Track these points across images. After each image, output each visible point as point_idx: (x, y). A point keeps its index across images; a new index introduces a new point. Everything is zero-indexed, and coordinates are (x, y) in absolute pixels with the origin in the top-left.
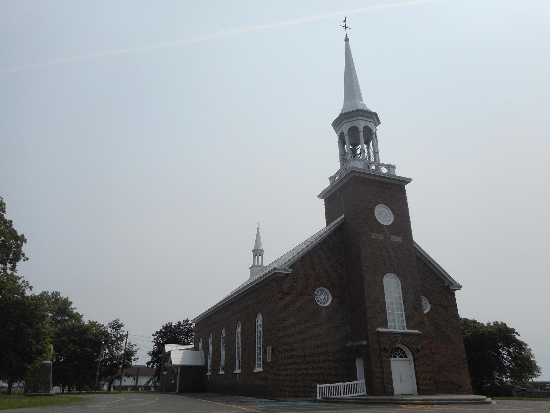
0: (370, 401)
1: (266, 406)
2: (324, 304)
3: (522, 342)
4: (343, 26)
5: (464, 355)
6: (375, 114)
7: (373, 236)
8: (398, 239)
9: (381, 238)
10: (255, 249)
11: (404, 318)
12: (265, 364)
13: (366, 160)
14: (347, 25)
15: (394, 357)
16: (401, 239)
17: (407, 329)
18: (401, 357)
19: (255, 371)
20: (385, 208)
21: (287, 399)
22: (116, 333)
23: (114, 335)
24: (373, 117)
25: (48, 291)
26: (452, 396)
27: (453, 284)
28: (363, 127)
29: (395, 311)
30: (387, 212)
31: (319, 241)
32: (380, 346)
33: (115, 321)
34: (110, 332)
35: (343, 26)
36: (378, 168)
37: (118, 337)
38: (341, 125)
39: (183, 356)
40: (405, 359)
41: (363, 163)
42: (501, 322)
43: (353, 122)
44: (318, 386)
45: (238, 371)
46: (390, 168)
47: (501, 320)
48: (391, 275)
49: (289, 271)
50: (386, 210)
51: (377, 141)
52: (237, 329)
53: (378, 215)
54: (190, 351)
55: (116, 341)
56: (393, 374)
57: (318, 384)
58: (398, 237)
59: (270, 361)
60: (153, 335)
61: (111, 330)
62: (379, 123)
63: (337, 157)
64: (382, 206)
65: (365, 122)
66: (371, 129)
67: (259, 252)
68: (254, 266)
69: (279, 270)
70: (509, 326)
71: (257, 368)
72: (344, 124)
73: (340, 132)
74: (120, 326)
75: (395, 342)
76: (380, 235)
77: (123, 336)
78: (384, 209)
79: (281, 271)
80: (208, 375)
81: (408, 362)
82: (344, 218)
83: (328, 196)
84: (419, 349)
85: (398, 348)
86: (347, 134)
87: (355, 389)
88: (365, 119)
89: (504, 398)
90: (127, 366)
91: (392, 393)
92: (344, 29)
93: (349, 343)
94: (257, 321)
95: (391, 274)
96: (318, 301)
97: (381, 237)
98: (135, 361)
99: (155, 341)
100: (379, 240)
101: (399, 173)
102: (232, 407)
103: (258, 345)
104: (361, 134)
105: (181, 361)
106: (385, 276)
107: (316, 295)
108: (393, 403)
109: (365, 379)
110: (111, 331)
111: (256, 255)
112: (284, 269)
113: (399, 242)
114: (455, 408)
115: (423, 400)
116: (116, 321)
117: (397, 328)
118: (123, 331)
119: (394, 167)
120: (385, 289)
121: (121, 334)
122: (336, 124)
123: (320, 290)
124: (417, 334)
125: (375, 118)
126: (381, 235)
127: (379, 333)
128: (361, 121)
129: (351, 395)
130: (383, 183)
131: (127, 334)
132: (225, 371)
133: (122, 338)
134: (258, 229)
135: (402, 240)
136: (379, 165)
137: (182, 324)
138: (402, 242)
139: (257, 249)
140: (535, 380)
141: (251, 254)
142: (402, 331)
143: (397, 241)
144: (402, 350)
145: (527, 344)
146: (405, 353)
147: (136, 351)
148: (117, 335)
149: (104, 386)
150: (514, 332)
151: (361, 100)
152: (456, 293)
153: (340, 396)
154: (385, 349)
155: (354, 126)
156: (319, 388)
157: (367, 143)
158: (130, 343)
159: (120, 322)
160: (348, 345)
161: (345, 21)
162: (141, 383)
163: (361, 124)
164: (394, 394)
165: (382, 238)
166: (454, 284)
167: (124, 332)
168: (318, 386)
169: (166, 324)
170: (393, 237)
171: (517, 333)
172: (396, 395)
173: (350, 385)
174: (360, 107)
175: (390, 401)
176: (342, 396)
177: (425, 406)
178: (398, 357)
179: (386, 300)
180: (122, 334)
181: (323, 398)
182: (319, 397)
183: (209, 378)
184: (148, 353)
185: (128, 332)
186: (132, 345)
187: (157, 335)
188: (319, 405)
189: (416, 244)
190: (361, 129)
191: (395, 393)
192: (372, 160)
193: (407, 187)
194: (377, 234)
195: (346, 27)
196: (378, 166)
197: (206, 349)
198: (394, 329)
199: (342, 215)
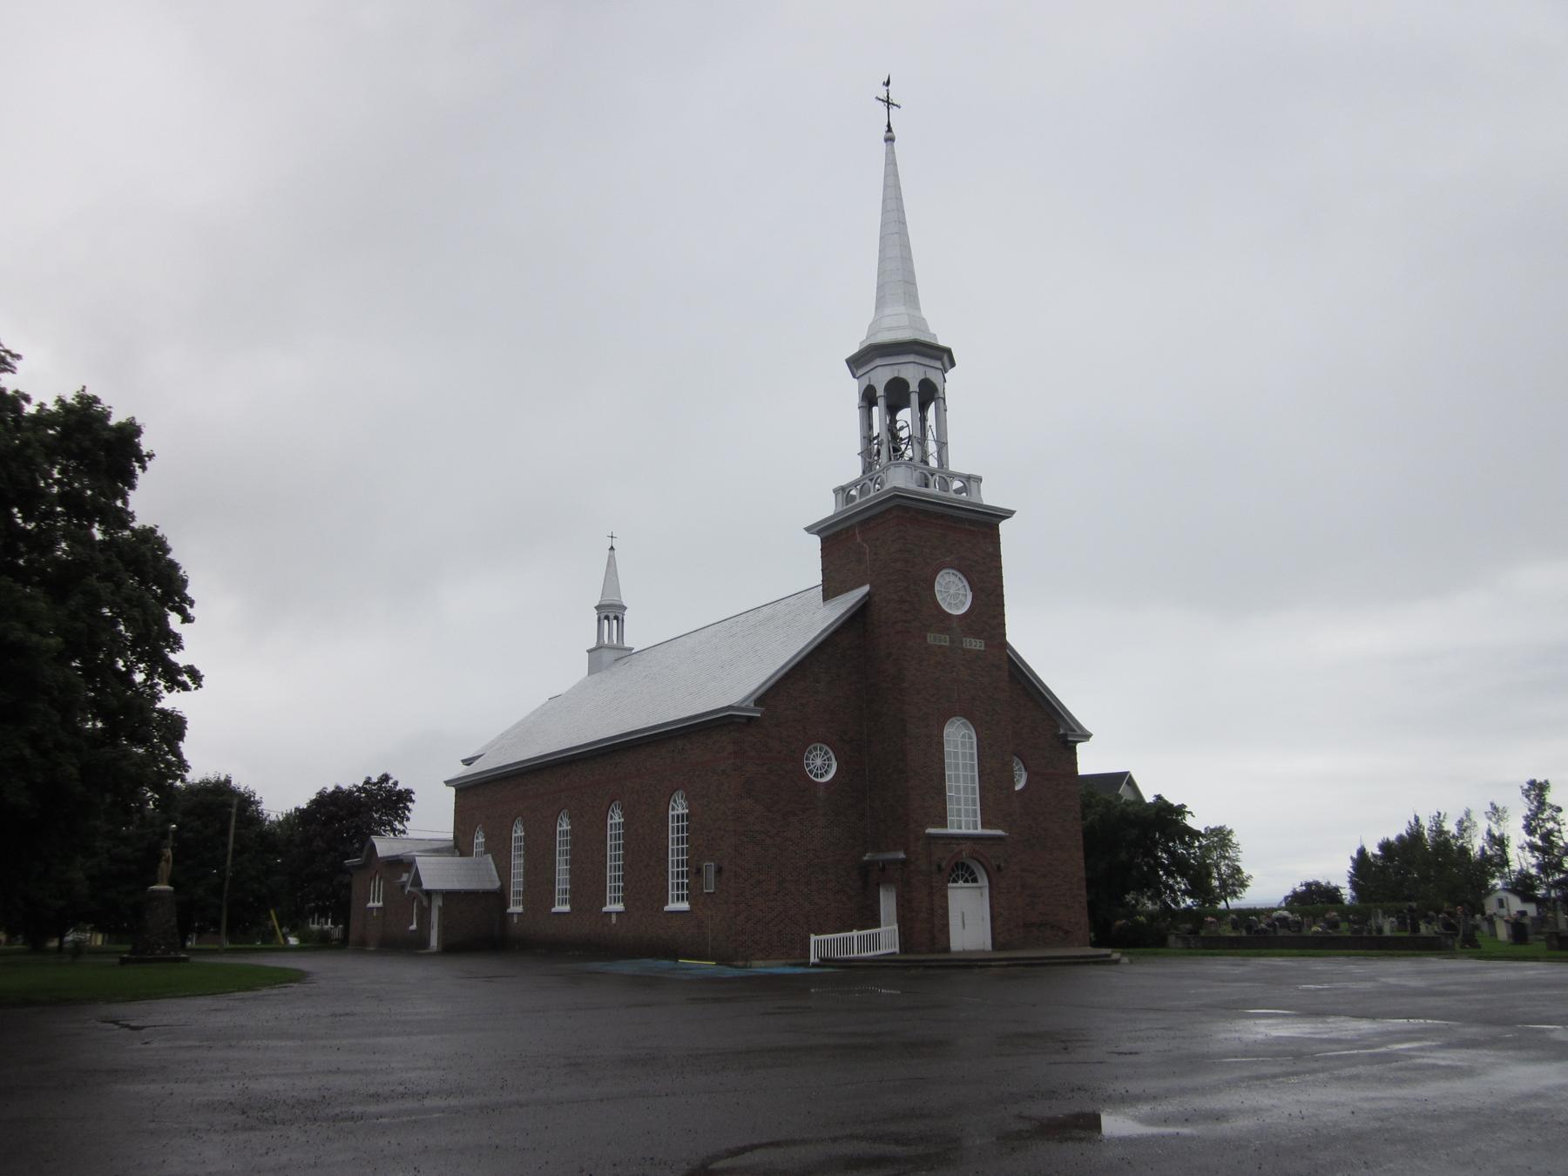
2: (821, 777)
5: (1083, 874)
6: (948, 352)
7: (928, 640)
8: (977, 645)
9: (943, 644)
14: (894, 98)
15: (955, 881)
16: (983, 644)
17: (983, 827)
18: (966, 881)
24: (942, 356)
27: (1074, 731)
28: (918, 381)
29: (962, 793)
30: (961, 585)
40: (974, 885)
43: (896, 367)
44: (813, 938)
50: (957, 580)
51: (946, 410)
56: (950, 914)
58: (978, 641)
59: (712, 891)
62: (953, 364)
64: (949, 573)
65: (922, 369)
68: (600, 647)
71: (673, 902)
73: (865, 382)
78: (953, 578)
80: (513, 914)
81: (978, 891)
82: (868, 594)
84: (1002, 865)
86: (882, 394)
91: (947, 949)
92: (882, 107)
96: (811, 771)
97: (944, 641)
100: (940, 647)
101: (990, 496)
124: (999, 838)
127: (931, 837)
135: (986, 645)
136: (947, 477)
138: (985, 651)
140: (1234, 903)
142: (971, 831)
144: (974, 874)
152: (1080, 747)
157: (923, 407)
161: (888, 83)
163: (912, 374)
164: (486, 894)
166: (1076, 729)
168: (813, 938)
175: (893, 964)
189: (1012, 648)
191: (497, 884)
192: (933, 463)
193: (1004, 527)
194: (938, 635)
195: (888, 103)
199: (863, 584)
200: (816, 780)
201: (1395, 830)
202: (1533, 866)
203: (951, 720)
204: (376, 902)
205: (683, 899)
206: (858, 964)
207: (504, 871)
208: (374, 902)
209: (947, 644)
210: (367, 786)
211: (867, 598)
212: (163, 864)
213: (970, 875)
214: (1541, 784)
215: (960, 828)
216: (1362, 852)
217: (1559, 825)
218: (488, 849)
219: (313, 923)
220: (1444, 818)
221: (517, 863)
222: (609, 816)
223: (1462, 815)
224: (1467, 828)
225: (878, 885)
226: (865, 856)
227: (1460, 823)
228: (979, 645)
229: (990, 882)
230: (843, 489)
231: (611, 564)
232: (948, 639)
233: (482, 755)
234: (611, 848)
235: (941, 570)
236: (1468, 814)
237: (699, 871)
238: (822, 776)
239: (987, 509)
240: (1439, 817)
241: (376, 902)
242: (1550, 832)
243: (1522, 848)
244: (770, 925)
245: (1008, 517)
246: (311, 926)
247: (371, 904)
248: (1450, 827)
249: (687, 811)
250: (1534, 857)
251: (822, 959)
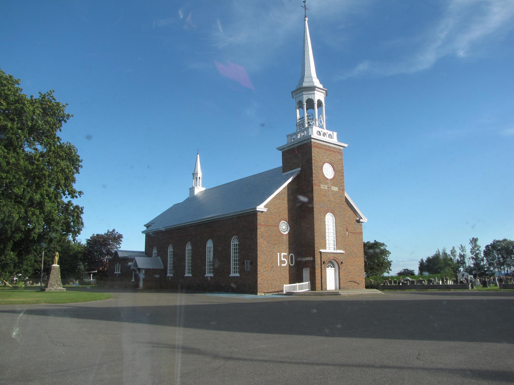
8: (335, 189)
9: (326, 188)
15: (328, 267)
25: (477, 238)
47: (486, 245)
50: (330, 167)
57: (284, 285)
58: (336, 188)
59: (249, 270)
65: (307, 95)
100: (325, 189)
124: (343, 253)
149: (37, 149)
153: (294, 291)
164: (161, 270)
168: (285, 285)
175: (329, 294)
176: (298, 291)
178: (330, 267)
191: (162, 267)
200: (283, 233)
201: (431, 254)
202: (472, 264)
204: (118, 272)
205: (211, 273)
206: (307, 294)
207: (165, 262)
208: (117, 272)
210: (108, 233)
212: (56, 257)
214: (475, 239)
216: (422, 260)
217: (480, 251)
218: (158, 254)
219: (85, 278)
220: (446, 249)
221: (170, 260)
222: (187, 244)
223: (452, 249)
224: (478, 253)
225: (303, 268)
226: (298, 259)
227: (451, 251)
230: (290, 135)
232: (327, 187)
233: (154, 223)
234: (187, 254)
236: (454, 248)
237: (243, 263)
238: (283, 231)
240: (444, 249)
241: (118, 272)
242: (478, 254)
243: (469, 258)
244: (269, 281)
246: (84, 279)
247: (115, 273)
248: (448, 252)
249: (239, 243)
250: (473, 261)
251: (287, 293)
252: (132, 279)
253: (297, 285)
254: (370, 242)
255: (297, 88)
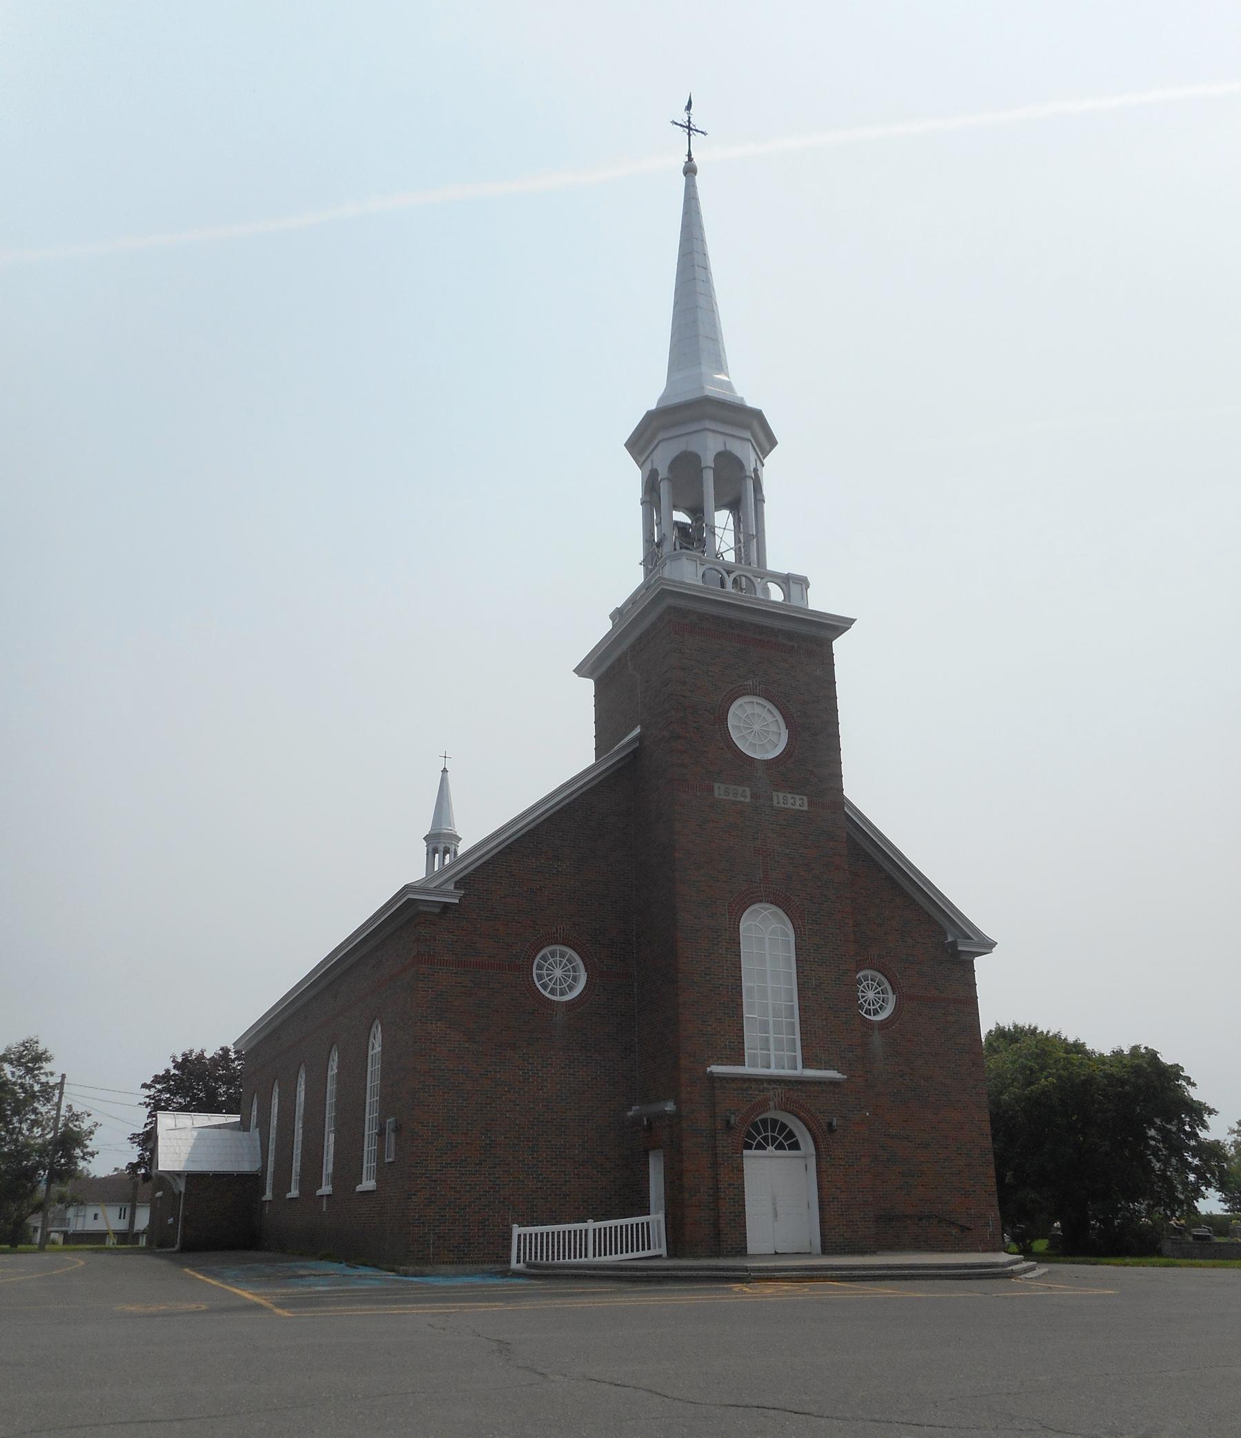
0: (650, 1273)
1: (340, 1288)
3: (1200, 1103)
4: (681, 125)
6: (758, 415)
7: (716, 794)
8: (798, 803)
10: (433, 832)
11: (798, 1036)
12: (382, 1172)
13: (717, 560)
15: (760, 1147)
17: (806, 1065)
18: (780, 1147)
19: (359, 1188)
20: (753, 702)
21: (428, 1269)
22: (28, 1080)
23: (22, 1086)
26: (915, 1257)
27: (970, 938)
28: (715, 454)
30: (770, 719)
31: (557, 808)
32: (715, 1116)
33: (23, 1045)
34: (9, 1076)
35: (681, 125)
36: (753, 587)
37: (35, 1092)
38: (652, 447)
39: (194, 1146)
41: (704, 568)
42: (1146, 1048)
44: (517, 1230)
45: (326, 1189)
46: (791, 583)
47: (1147, 1041)
48: (765, 909)
49: (454, 897)
50: (765, 714)
52: (329, 1070)
53: (738, 727)
54: (227, 1133)
55: (25, 1102)
58: (797, 797)
60: (145, 1086)
61: (14, 1070)
62: (773, 442)
63: (637, 551)
65: (720, 438)
66: (740, 460)
67: (445, 843)
69: (419, 893)
70: (1167, 1058)
72: (658, 444)
73: (648, 466)
74: (39, 1058)
75: (763, 1105)
76: (740, 789)
77: (50, 1087)
78: (758, 710)
79: (428, 894)
82: (640, 738)
83: (603, 669)
84: (835, 1123)
85: (775, 1122)
87: (641, 1237)
88: (723, 430)
89: (1128, 1260)
90: (65, 1174)
91: (741, 1251)
92: (683, 133)
93: (634, 1108)
94: (370, 1044)
95: (768, 905)
96: (545, 986)
97: (743, 795)
98: (86, 1160)
99: (150, 1104)
101: (819, 601)
102: (227, 1291)
103: (371, 1116)
104: (709, 478)
105: (188, 1160)
106: (747, 912)
107: (540, 967)
108: (585, 1276)
109: (665, 1210)
110: (13, 1073)
111: (435, 851)
112: (438, 890)
113: (799, 811)
114: (884, 1291)
115: (806, 1268)
116: (27, 1045)
117: (773, 1065)
118: (50, 1072)
119: (803, 582)
120: (744, 949)
121: (42, 1081)
122: (639, 444)
123: (553, 954)
124: (833, 1083)
125: (756, 425)
126: (744, 791)
127: (712, 1078)
128: (710, 435)
129: (620, 1257)
130: (760, 629)
131: (62, 1084)
132: (300, 1191)
133: (47, 1091)
134: (445, 771)
135: (810, 804)
137: (233, 1056)
139: (437, 831)
141: (423, 847)
142: (787, 1072)
143: (793, 807)
145: (1217, 1110)
146: (795, 1136)
147: (91, 1133)
148: (32, 1086)
150: (1178, 1077)
151: (720, 366)
152: (978, 962)
153: (603, 1258)
154: (728, 1126)
155: (689, 450)
156: (519, 1236)
158: (70, 1107)
159: (41, 1048)
160: (630, 1114)
161: (689, 107)
162: (108, 1224)
163: (710, 446)
165: (745, 797)
167: (52, 1074)
168: (517, 1230)
169: (183, 1055)
170: (781, 795)
171: (1188, 1079)
172: (754, 1256)
173: (643, 1224)
174: (712, 391)
175: (708, 1273)
176: (591, 1259)
177: (797, 1286)
178: (770, 1148)
179: (745, 984)
180: (47, 1083)
181: (529, 1266)
182: (518, 1261)
183: (325, 1206)
184: (131, 1139)
185: (63, 1076)
186: (77, 1116)
187: (155, 1087)
188: (503, 1285)
190: (708, 460)
193: (840, 646)
196: (752, 578)
197: (263, 1124)
198: (763, 1067)
199: (635, 727)
203: (750, 909)
209: (748, 800)
211: (637, 744)
213: (786, 1138)
215: (768, 1067)
225: (646, 1153)
228: (798, 802)
229: (817, 1148)
231: (444, 781)
235: (740, 696)
239: (815, 616)
245: (848, 629)
252: (264, 1193)
253: (586, 1231)
254: (991, 1031)
255: (659, 406)
